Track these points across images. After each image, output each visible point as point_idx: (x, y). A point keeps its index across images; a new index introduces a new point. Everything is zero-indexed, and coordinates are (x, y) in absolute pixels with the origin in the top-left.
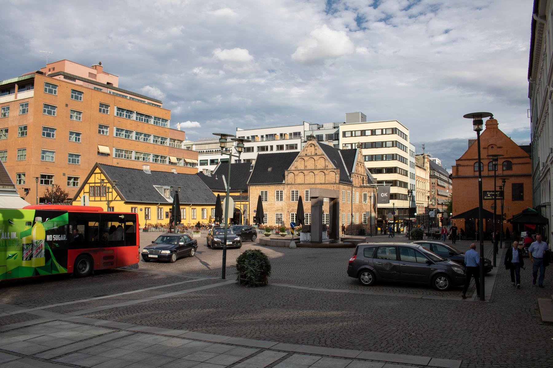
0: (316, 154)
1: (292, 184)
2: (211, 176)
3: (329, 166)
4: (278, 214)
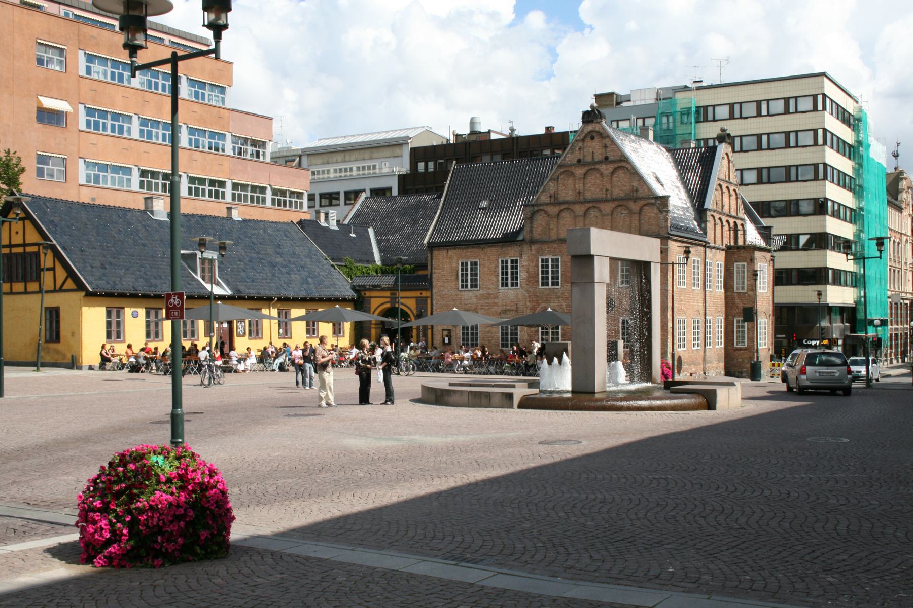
1: (542, 242)
2: (336, 228)
3: (641, 190)
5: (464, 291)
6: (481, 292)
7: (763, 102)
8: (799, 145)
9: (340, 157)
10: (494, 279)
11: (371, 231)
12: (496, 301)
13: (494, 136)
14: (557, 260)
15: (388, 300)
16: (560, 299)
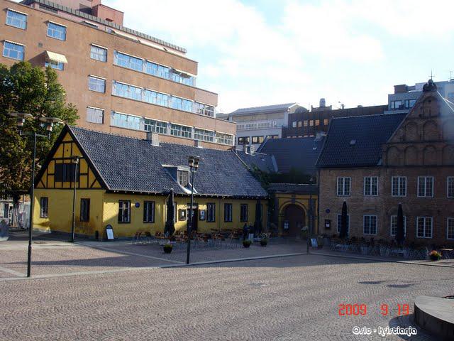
9: (250, 118)
11: (163, 166)
14: (404, 179)
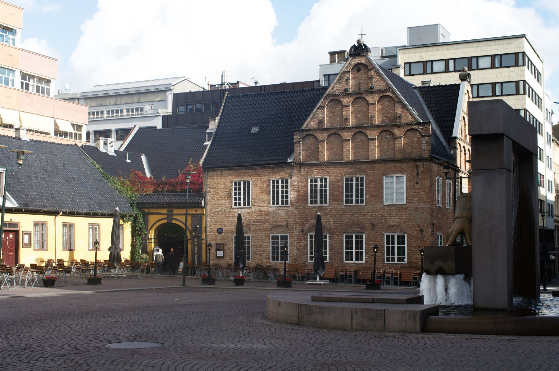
0: (371, 88)
3: (404, 117)
4: (278, 237)
5: (238, 208)
6: (253, 209)
7: (473, 59)
8: (504, 94)
9: (112, 101)
10: (266, 198)
11: (143, 158)
12: (267, 217)
13: (241, 86)
15: (165, 216)
16: (328, 216)
